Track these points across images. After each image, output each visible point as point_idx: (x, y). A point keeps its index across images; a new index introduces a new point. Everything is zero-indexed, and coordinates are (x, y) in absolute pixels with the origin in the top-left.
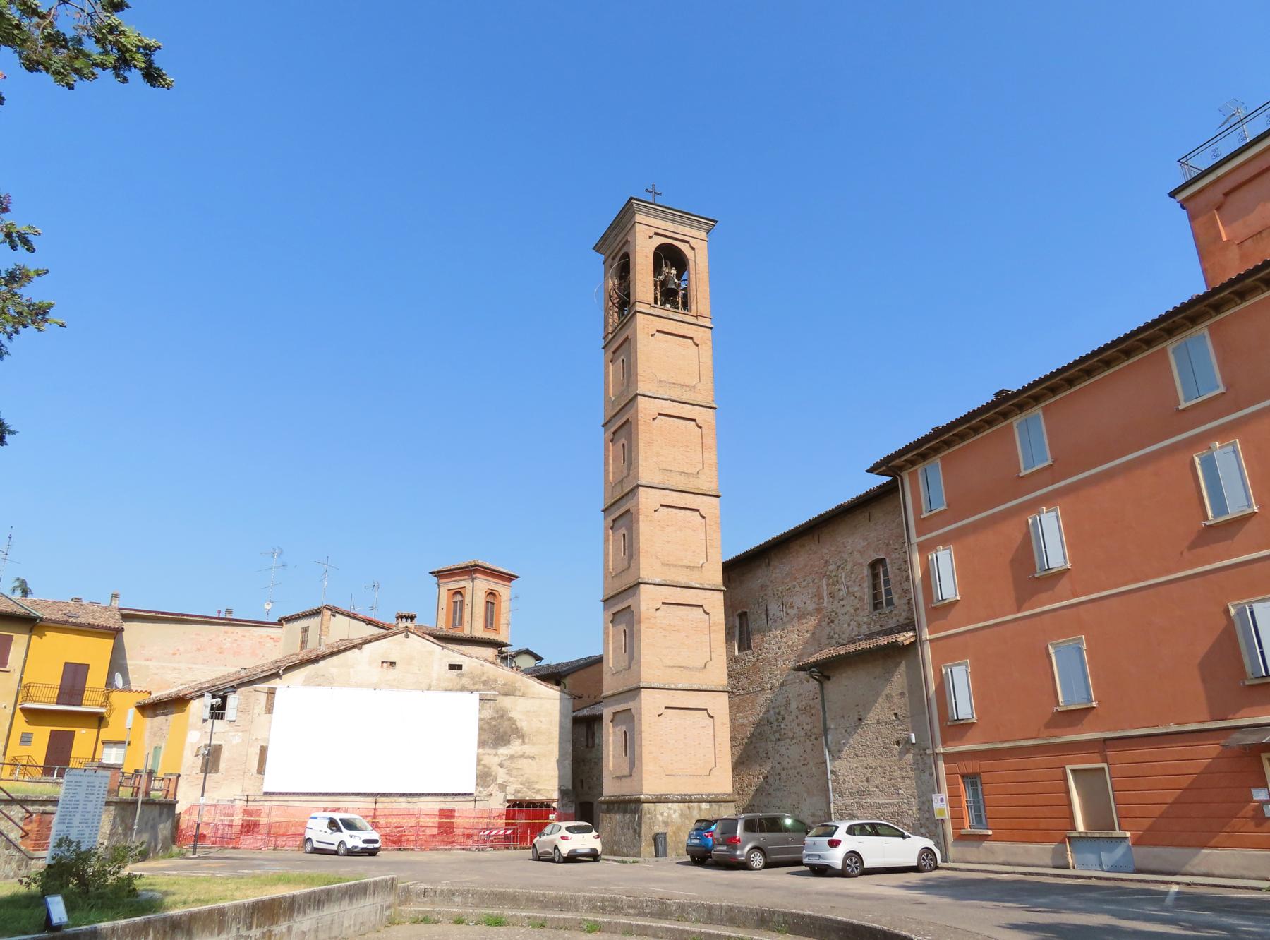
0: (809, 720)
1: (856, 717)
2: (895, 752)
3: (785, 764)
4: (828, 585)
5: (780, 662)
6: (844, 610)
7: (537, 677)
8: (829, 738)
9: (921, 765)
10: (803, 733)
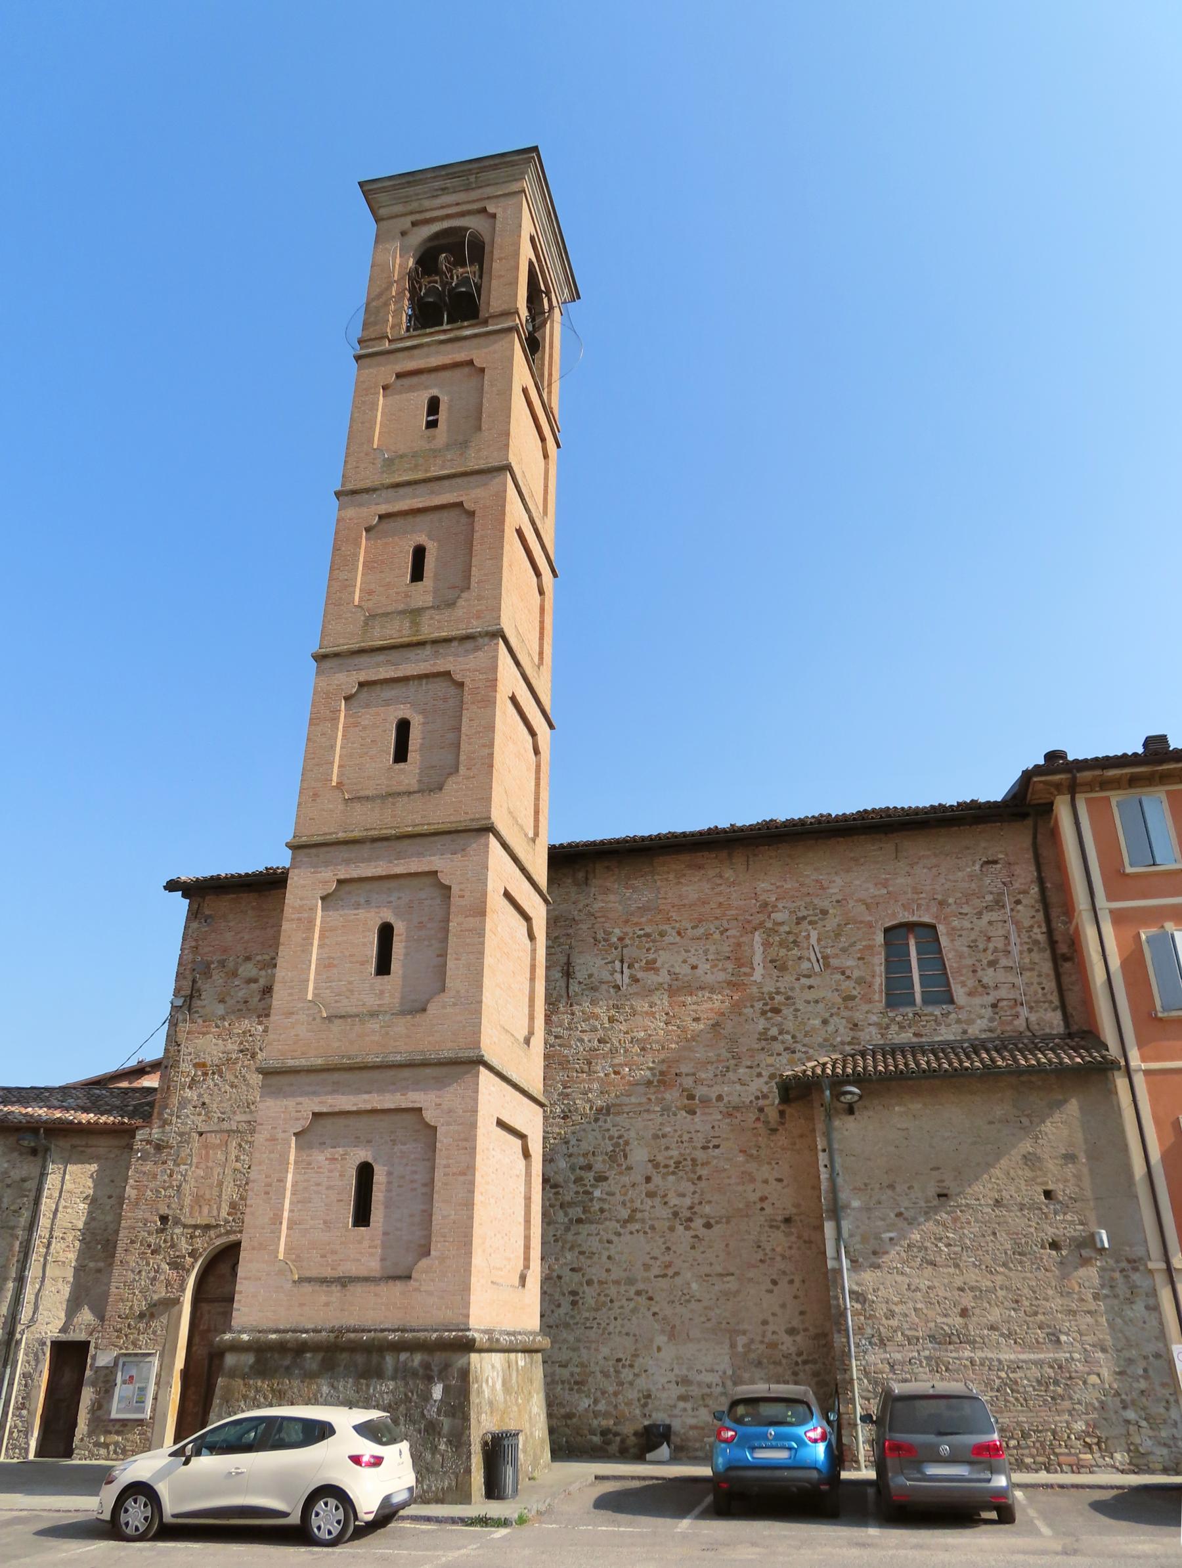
0: (687, 1187)
1: (932, 1191)
3: (596, 1273)
4: (766, 945)
5: (602, 1068)
8: (846, 1225)
9: (1122, 1290)
10: (665, 1213)
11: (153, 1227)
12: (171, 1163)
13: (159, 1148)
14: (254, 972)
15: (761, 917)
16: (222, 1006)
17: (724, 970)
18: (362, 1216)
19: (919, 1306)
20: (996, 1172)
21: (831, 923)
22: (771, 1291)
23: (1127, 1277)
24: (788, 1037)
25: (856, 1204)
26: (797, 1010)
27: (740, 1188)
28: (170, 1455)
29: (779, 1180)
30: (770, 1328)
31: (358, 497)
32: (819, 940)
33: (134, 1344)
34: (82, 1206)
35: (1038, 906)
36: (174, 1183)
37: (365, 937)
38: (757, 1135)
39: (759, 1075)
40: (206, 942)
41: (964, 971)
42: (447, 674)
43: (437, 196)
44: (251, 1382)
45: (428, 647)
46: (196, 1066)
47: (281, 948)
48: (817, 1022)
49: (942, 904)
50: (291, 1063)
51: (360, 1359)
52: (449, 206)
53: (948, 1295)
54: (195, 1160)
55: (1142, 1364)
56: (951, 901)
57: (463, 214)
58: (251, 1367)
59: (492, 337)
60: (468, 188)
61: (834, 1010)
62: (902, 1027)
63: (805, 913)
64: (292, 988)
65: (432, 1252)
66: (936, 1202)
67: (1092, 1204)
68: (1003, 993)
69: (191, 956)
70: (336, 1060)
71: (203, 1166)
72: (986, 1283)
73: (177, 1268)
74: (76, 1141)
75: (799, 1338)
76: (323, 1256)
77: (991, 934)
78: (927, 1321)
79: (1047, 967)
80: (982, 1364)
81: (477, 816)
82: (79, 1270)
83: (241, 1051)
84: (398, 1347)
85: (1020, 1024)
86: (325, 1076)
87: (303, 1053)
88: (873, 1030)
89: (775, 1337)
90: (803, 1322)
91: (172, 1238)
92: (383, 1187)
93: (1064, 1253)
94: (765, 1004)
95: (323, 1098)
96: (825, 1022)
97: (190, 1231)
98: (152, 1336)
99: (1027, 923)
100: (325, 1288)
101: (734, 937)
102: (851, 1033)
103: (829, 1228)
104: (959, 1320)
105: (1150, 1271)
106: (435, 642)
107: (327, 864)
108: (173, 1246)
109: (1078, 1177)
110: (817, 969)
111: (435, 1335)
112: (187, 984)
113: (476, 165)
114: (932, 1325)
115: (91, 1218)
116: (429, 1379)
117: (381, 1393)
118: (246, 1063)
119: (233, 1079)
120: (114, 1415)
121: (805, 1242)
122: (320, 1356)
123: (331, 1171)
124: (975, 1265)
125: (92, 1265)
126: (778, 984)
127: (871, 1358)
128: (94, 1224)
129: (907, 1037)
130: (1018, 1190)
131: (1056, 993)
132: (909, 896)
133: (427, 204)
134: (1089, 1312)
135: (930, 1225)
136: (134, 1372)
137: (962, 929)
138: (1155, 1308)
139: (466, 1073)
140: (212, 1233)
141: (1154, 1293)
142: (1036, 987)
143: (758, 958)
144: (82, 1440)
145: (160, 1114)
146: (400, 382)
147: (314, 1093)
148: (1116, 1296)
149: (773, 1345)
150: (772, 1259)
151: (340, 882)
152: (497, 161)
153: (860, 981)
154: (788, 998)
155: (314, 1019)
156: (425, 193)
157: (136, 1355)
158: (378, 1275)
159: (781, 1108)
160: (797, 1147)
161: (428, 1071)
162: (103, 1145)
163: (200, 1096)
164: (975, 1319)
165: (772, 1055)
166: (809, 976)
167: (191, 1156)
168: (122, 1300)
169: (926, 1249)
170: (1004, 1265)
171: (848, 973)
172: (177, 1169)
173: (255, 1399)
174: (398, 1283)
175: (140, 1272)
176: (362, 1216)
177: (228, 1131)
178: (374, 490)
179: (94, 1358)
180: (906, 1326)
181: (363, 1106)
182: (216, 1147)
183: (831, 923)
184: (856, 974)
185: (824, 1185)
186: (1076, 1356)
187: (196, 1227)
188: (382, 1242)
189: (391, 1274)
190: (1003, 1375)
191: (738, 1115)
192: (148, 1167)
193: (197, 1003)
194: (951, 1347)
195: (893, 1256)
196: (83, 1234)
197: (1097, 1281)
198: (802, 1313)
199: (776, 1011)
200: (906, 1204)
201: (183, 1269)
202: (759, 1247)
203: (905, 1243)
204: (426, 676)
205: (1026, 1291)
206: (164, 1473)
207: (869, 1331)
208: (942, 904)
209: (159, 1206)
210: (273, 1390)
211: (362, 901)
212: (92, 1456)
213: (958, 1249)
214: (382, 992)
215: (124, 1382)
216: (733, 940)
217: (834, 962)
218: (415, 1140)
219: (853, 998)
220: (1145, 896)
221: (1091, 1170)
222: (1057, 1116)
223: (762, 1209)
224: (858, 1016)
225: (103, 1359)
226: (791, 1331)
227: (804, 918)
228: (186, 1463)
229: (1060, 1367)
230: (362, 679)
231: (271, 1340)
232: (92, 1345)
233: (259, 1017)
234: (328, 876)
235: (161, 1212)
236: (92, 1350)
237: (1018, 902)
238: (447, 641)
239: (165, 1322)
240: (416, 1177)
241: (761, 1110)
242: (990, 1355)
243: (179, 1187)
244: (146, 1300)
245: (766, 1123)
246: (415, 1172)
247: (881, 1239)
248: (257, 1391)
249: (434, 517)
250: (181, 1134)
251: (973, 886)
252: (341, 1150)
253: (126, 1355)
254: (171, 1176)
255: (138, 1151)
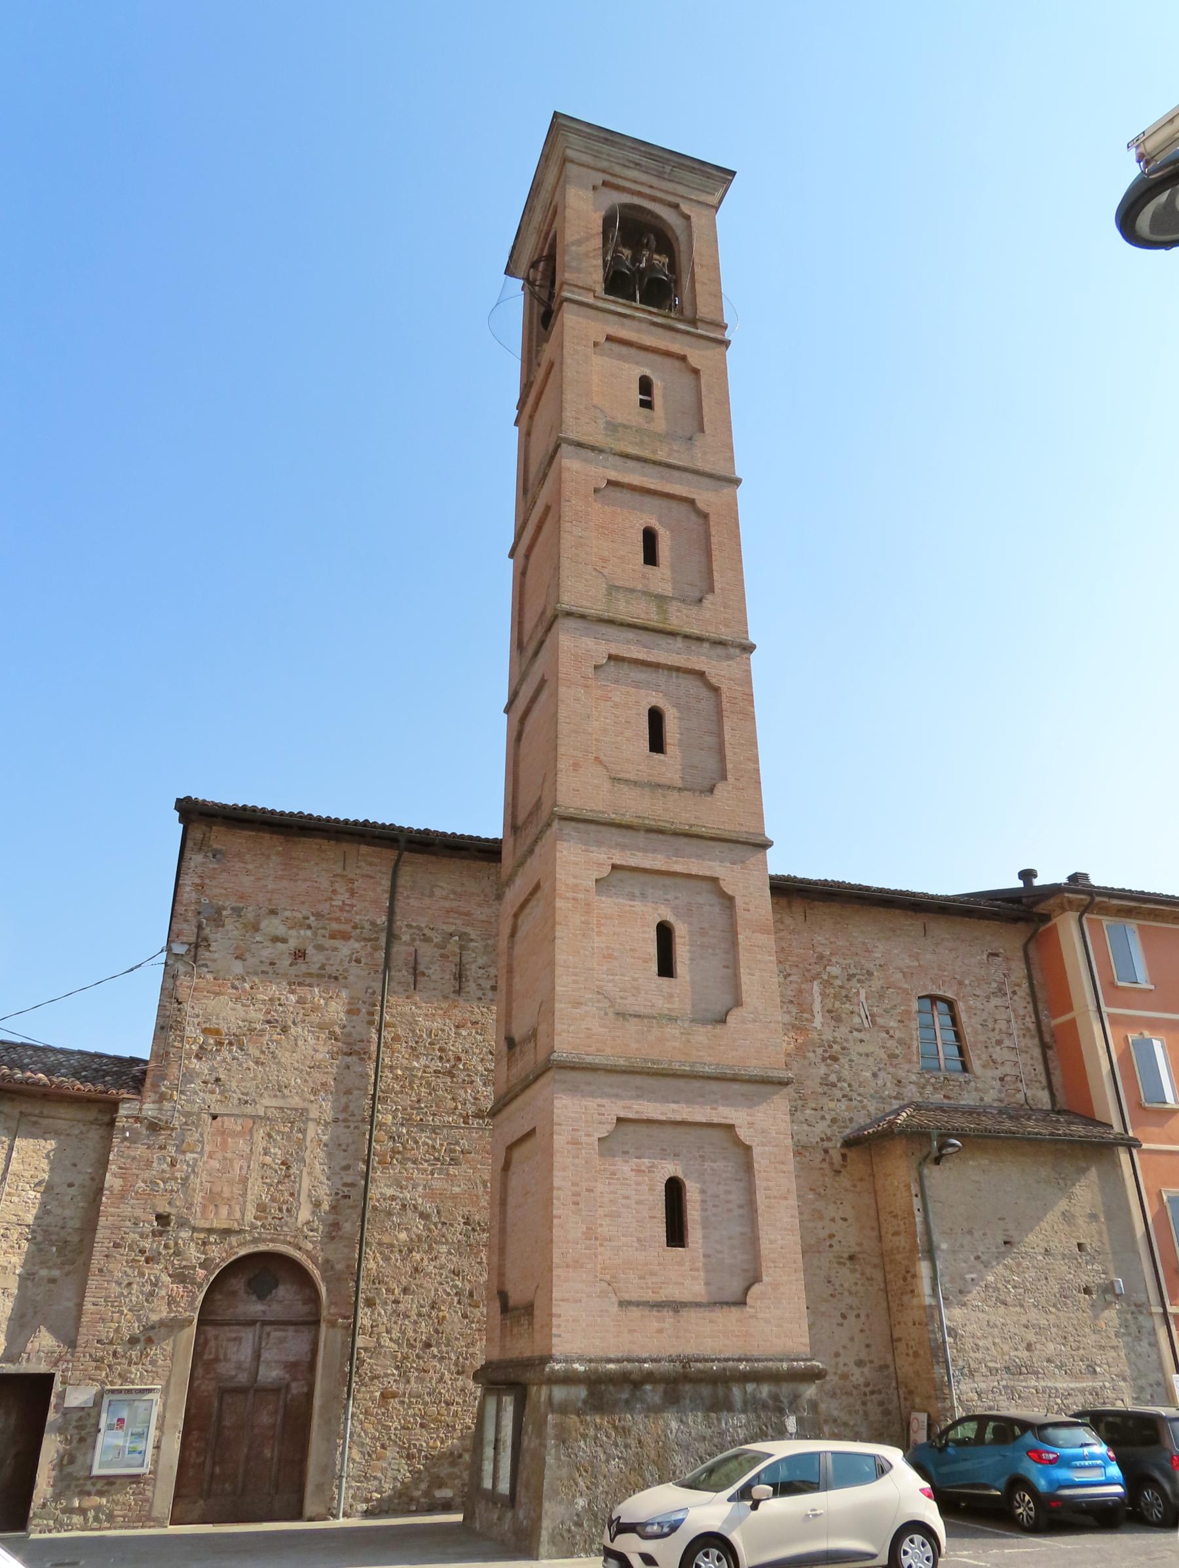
1: (1000, 1240)
2: (1084, 1305)
4: (823, 995)
6: (862, 1048)
7: (683, 1486)
9: (1133, 1329)
11: (147, 1228)
12: (172, 1150)
13: (154, 1127)
14: (281, 930)
15: (818, 968)
16: (239, 963)
17: (789, 1012)
18: (676, 1234)
19: (997, 1340)
20: (1043, 1224)
21: (876, 984)
22: (842, 1325)
23: (1136, 1318)
24: (846, 1085)
25: (944, 1246)
26: (851, 1061)
27: (811, 1225)
28: (729, 1500)
29: (845, 1219)
30: (841, 1360)
31: (583, 451)
32: (867, 998)
33: (123, 1377)
34: (32, 1194)
35: (1029, 999)
36: (178, 1175)
37: (644, 932)
38: (823, 1175)
39: (823, 1118)
40: (214, 883)
41: (979, 1046)
42: (701, 675)
43: (628, 167)
44: (588, 1418)
45: (679, 639)
46: (205, 1031)
47: (558, 927)
48: (868, 1074)
49: (961, 983)
50: (589, 1059)
51: (706, 1390)
52: (642, 184)
53: (1017, 1331)
54: (207, 1148)
55: (1149, 1391)
56: (967, 982)
57: (654, 199)
58: (585, 1402)
59: (702, 342)
60: (660, 176)
61: (882, 1066)
62: (935, 1089)
63: (855, 971)
64: (576, 975)
65: (765, 1278)
66: (1003, 1249)
67: (1110, 1256)
68: (1008, 1069)
69: (194, 895)
70: (640, 1064)
71: (219, 1156)
72: (1043, 1322)
73: (183, 1281)
74: (27, 1108)
75: (866, 1370)
76: (642, 1277)
77: (997, 1017)
78: (1003, 1354)
79: (1037, 1052)
80: (1044, 1392)
81: (751, 830)
82: (27, 1278)
83: (269, 1022)
84: (745, 1378)
85: (1020, 1097)
86: (625, 1078)
87: (598, 1050)
88: (913, 1088)
89: (846, 1369)
90: (869, 1354)
91: (176, 1244)
92: (698, 1206)
93: (1094, 1297)
94: (825, 1051)
95: (628, 1103)
96: (875, 1075)
97: (202, 1236)
98: (150, 1368)
99: (1022, 1012)
100: (655, 1313)
101: (797, 982)
102: (897, 1089)
103: (924, 1268)
104: (1026, 1353)
105: (1151, 1314)
106: (687, 637)
107: (599, 844)
108: (177, 1253)
109: (1100, 1233)
110: (866, 1025)
111: (785, 1365)
112: (189, 931)
113: (676, 159)
114: (1007, 1357)
115: (44, 1211)
116: (781, 1411)
117: (735, 1427)
118: (275, 1037)
119: (257, 1053)
120: (96, 1471)
121: (868, 1279)
122: (661, 1388)
123: (638, 1184)
124: (1035, 1306)
125: (44, 1272)
126: (835, 1034)
127: (963, 1387)
128: (48, 1219)
129: (938, 1098)
130: (1061, 1242)
131: (1044, 1075)
132: (936, 971)
133: (618, 170)
134: (1113, 1347)
135: (1000, 1269)
136: (124, 1414)
137: (976, 1008)
138: (1155, 1344)
139: (774, 1094)
140: (234, 1240)
141: (1154, 1332)
142: (1029, 1068)
143: (817, 1007)
144: (44, 1505)
145: (155, 1086)
146: (608, 345)
147: (617, 1096)
148: (1129, 1334)
149: (845, 1377)
150: (841, 1294)
151: (614, 867)
152: (696, 165)
153: (901, 1042)
154: (844, 1048)
155: (606, 1014)
156: (618, 158)
157: (129, 1391)
158: (704, 1300)
159: (843, 1151)
160: (858, 1189)
161: (736, 1086)
162: (64, 1117)
163: (212, 1069)
164: (1037, 1352)
165: (832, 1100)
166: (859, 1031)
167: (202, 1142)
168: (103, 1320)
169: (999, 1290)
170: (1054, 1306)
171: (891, 1032)
172: (180, 1157)
173: (596, 1438)
174: (733, 1309)
175: (129, 1284)
176: (676, 1234)
177: (255, 1118)
178: (601, 451)
179: (62, 1396)
180: (988, 1358)
181: (672, 1116)
182: (234, 1134)
183: (876, 984)
184: (898, 1035)
185: (920, 1228)
186: (1107, 1384)
187: (210, 1231)
188: (704, 1264)
189: (717, 1300)
190: (1059, 1401)
191: (807, 1154)
192: (140, 1150)
193: (204, 954)
194: (1021, 1377)
195: (974, 1296)
196: (33, 1232)
197: (1117, 1322)
198: (868, 1346)
199: (835, 1059)
200: (982, 1248)
201: (193, 1283)
202: (829, 1282)
203: (983, 1284)
204: (678, 669)
205: (1071, 1329)
206: (733, 1521)
207: (961, 1363)
208: (961, 983)
209: (157, 1201)
210: (615, 1427)
211: (637, 892)
212: (59, 1526)
213: (1021, 1291)
214: (671, 996)
215: (110, 1427)
216: (795, 986)
217: (880, 1021)
218: (725, 1158)
219: (896, 1056)
220: (1128, 1007)
221: (1109, 1230)
222: (1083, 1182)
223: (831, 1246)
224: (901, 1074)
225: (78, 1397)
226: (860, 1363)
227: (854, 975)
228: (755, 1507)
229: (1097, 1394)
230: (613, 652)
231: (610, 1371)
232: (58, 1379)
233: (290, 984)
234: (604, 856)
235: (160, 1210)
236: (57, 1387)
237: (1014, 993)
238: (700, 639)
239: (169, 1349)
240: (732, 1197)
241: (826, 1151)
242: (1050, 1384)
243: (185, 1180)
244: (139, 1320)
245: (831, 1164)
246: (728, 1192)
247: (965, 1279)
248: (598, 1428)
249: (665, 503)
250: (187, 1115)
251: (983, 973)
252: (646, 1161)
253: (113, 1391)
254: (173, 1165)
255: (124, 1129)
